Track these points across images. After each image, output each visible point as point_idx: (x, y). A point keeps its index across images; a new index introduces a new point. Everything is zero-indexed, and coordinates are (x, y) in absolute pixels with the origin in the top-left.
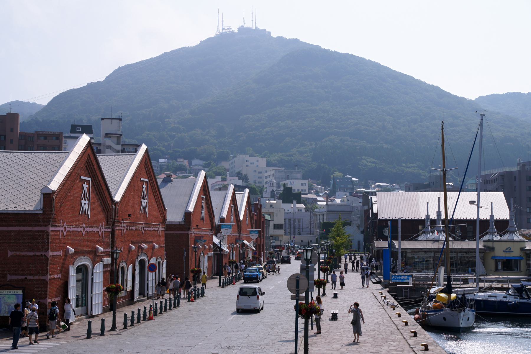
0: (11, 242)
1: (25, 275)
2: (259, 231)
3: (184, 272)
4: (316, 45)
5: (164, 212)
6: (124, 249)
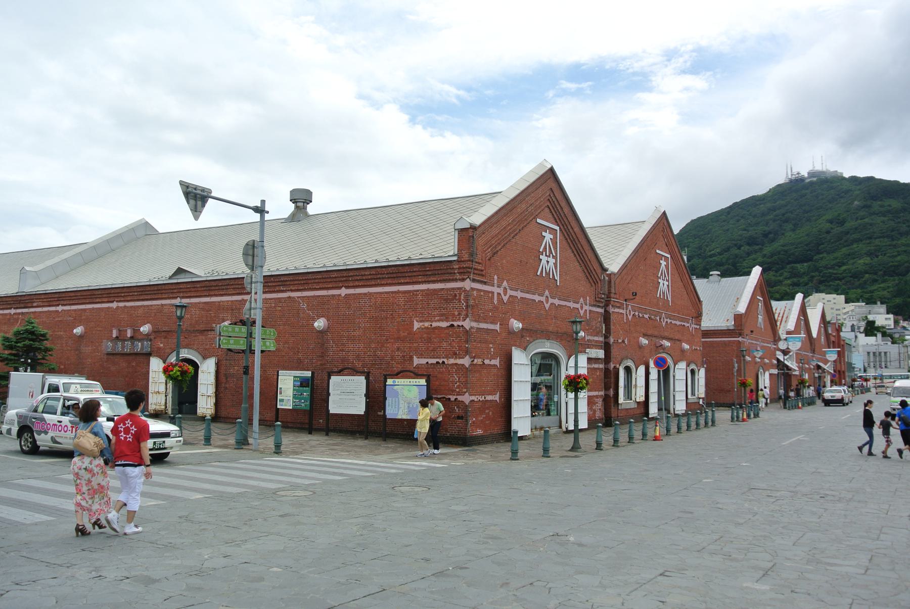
0: (418, 308)
1: (437, 358)
2: (838, 351)
3: (736, 390)
4: (894, 181)
5: (699, 305)
6: (630, 342)
